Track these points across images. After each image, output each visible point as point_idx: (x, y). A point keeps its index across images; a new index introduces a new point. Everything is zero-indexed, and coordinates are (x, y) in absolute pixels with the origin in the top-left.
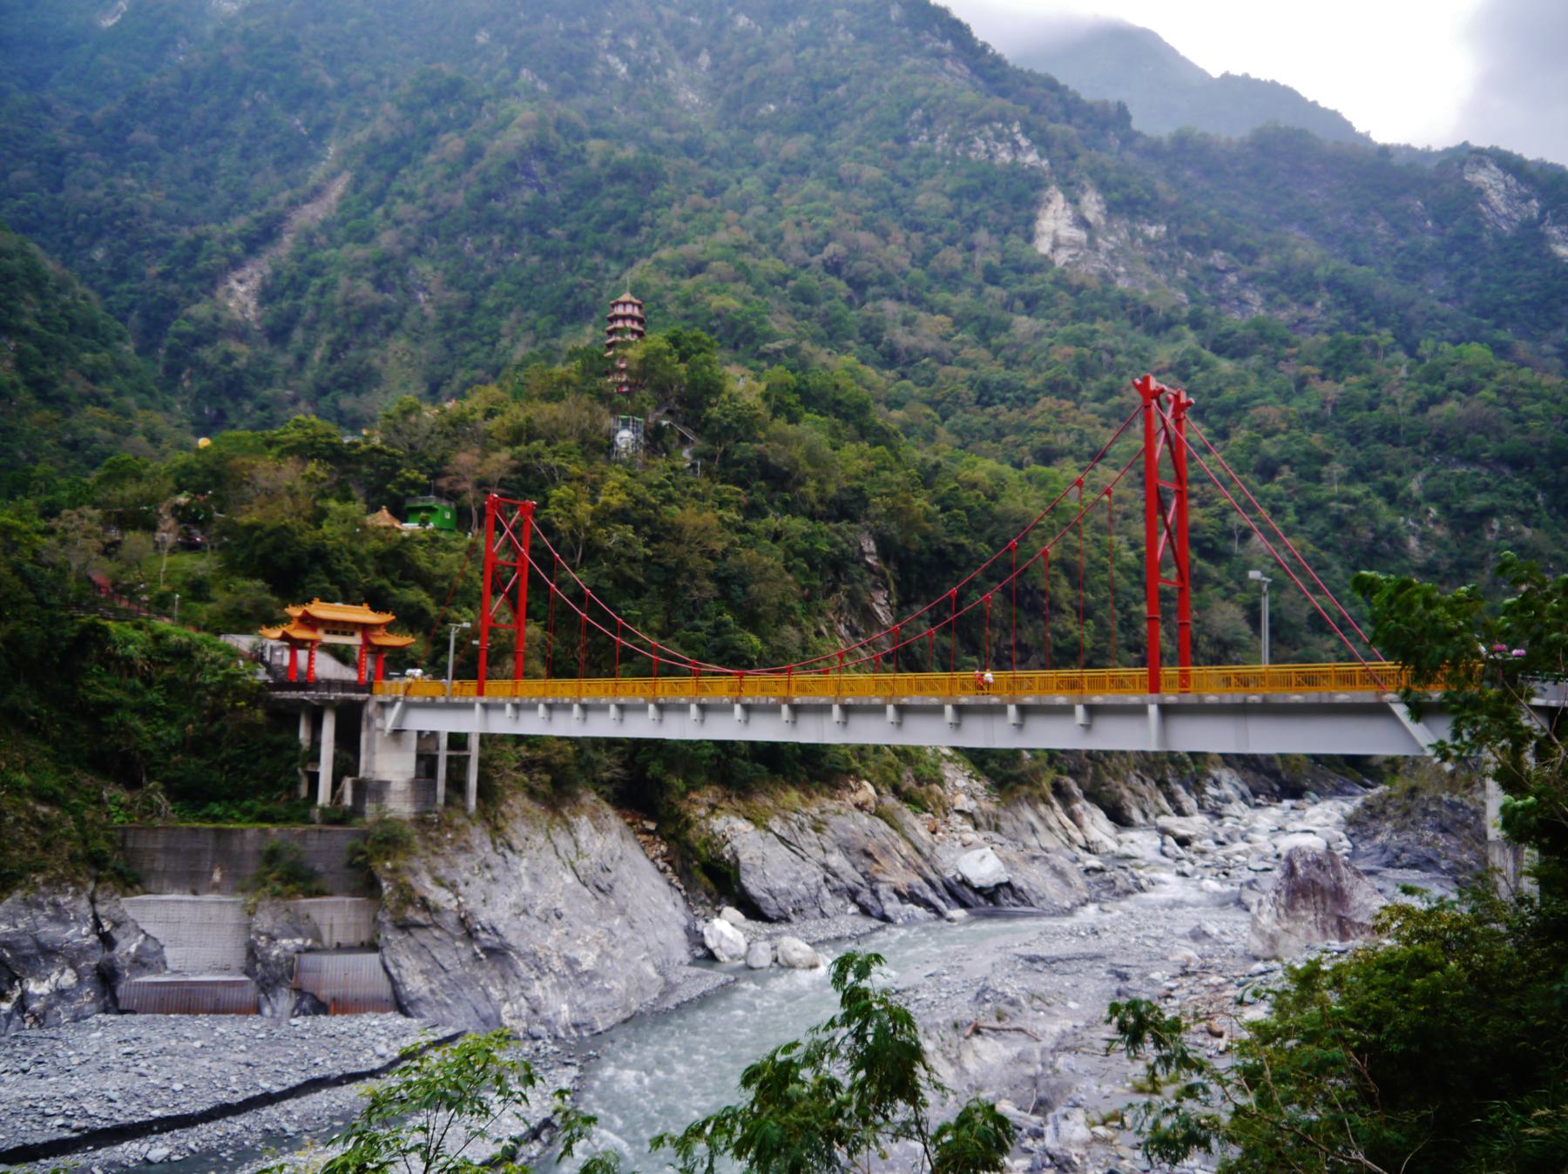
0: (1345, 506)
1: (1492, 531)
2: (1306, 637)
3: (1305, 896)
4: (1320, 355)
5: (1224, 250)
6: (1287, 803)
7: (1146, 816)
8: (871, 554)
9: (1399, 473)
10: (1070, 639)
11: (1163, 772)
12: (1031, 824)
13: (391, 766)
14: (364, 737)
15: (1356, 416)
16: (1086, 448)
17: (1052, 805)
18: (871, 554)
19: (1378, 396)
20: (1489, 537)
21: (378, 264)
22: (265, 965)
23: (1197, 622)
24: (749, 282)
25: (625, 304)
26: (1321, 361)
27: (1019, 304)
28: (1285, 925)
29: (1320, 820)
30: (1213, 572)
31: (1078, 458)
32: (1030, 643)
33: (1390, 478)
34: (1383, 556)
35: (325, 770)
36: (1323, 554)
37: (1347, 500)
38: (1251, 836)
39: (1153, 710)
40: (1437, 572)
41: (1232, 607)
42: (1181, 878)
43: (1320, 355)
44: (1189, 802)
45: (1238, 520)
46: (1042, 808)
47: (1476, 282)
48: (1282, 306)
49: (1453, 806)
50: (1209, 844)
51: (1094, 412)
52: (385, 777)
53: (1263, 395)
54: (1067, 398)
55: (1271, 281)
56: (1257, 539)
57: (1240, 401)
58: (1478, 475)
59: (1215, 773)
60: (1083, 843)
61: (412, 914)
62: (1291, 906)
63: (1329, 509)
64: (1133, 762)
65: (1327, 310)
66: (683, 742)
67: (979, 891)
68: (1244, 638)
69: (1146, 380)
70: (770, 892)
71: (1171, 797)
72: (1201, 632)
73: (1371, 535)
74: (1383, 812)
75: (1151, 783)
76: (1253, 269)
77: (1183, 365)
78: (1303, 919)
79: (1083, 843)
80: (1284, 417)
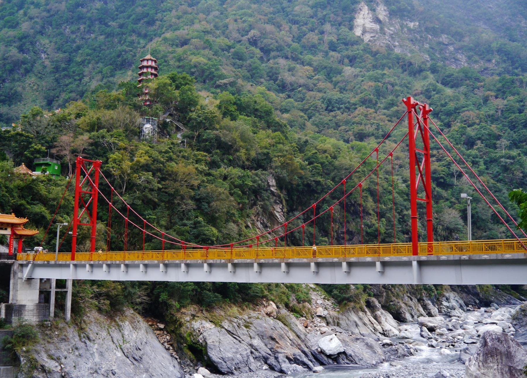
0: (508, 160)
2: (490, 226)
4: (495, 86)
5: (447, 34)
6: (483, 309)
7: (413, 317)
8: (273, 186)
10: (373, 228)
11: (421, 295)
12: (356, 322)
15: (513, 116)
16: (381, 132)
17: (366, 312)
18: (273, 186)
19: (523, 106)
21: (20, 39)
23: (437, 219)
24: (211, 49)
25: (148, 60)
26: (495, 89)
27: (346, 61)
28: (482, 371)
30: (444, 193)
31: (377, 138)
32: (354, 230)
36: (498, 184)
37: (509, 157)
38: (465, 326)
39: (415, 263)
41: (454, 211)
42: (431, 348)
43: (495, 86)
44: (434, 310)
45: (455, 167)
46: (361, 314)
48: (476, 62)
50: (444, 330)
51: (384, 115)
52: (23, 303)
53: (467, 106)
54: (371, 108)
55: (471, 49)
57: (456, 109)
59: (447, 295)
60: (381, 331)
62: (485, 361)
63: (500, 162)
64: (406, 290)
65: (498, 64)
67: (329, 356)
68: (459, 226)
70: (223, 359)
71: (425, 307)
72: (439, 224)
73: (521, 175)
75: (415, 300)
76: (462, 43)
77: (427, 90)
78: (491, 368)
79: (381, 331)
80: (478, 117)
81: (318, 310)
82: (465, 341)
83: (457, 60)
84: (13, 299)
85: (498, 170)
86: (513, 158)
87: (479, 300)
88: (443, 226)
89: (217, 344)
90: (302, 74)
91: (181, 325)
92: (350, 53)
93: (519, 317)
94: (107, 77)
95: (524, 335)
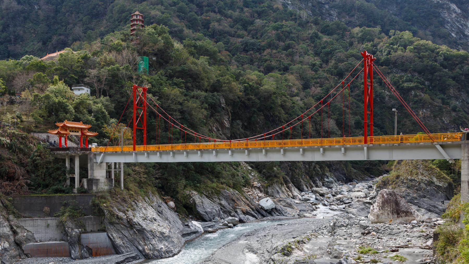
3: (387, 203)
13: (99, 174)
14: (89, 165)
22: (71, 237)
24: (162, 5)
25: (137, 15)
27: (256, 15)
29: (361, 187)
31: (280, 70)
35: (77, 176)
39: (365, 148)
41: (331, 120)
44: (320, 183)
47: (406, 8)
48: (344, 17)
50: (330, 195)
52: (98, 178)
60: (292, 196)
61: (114, 220)
66: (209, 163)
67: (266, 211)
69: (365, 52)
70: (206, 212)
77: (311, 38)
81: (254, 183)
83: (331, 15)
84: (91, 176)
89: (201, 204)
90: (225, 25)
91: (178, 193)
92: (259, 10)
94: (86, 24)
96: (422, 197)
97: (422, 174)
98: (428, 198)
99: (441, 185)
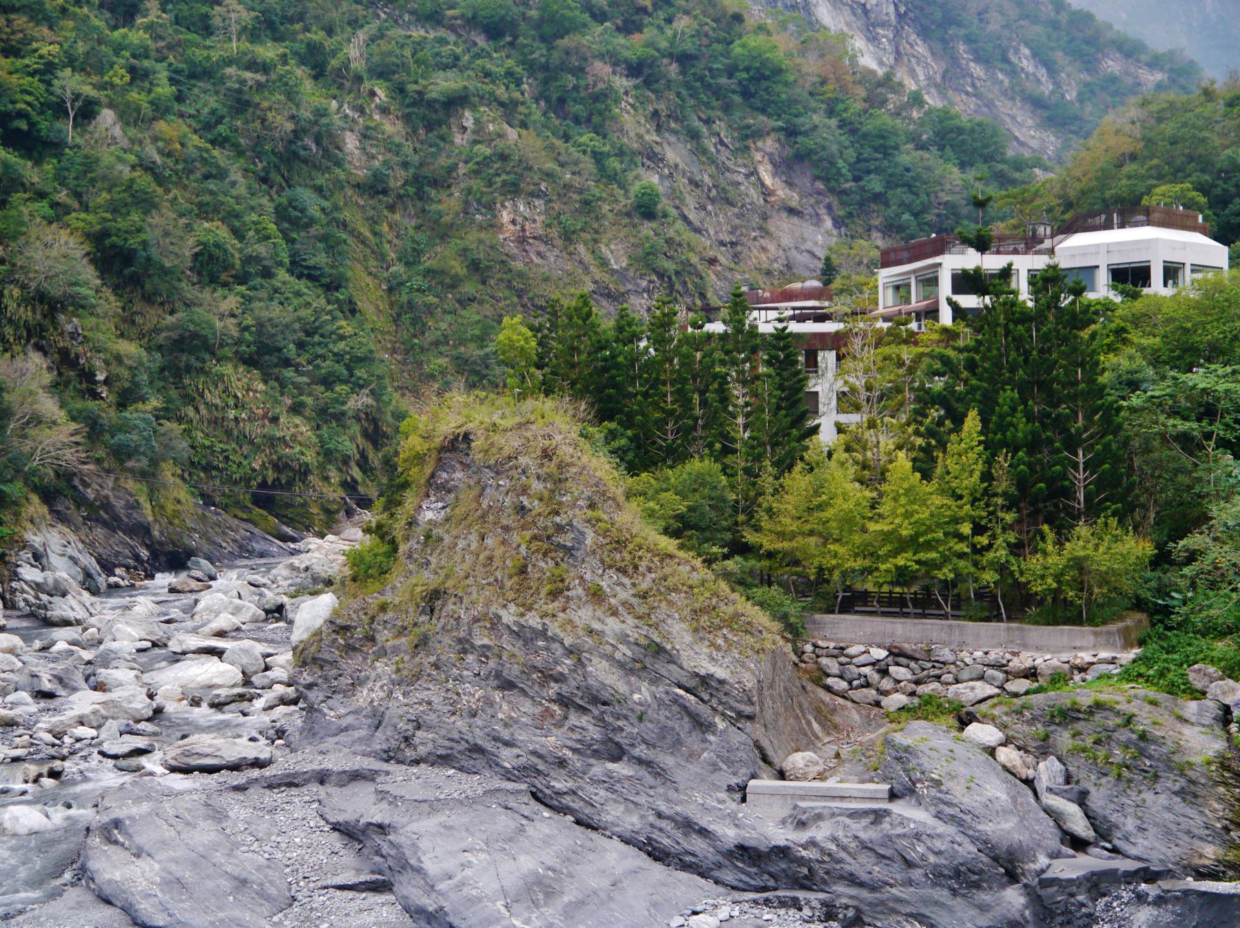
0: (248, 75)
1: (465, 129)
6: (164, 579)
9: (330, 31)
20: (458, 139)
33: (317, 36)
34: (305, 162)
36: (216, 153)
37: (252, 65)
40: (385, 192)
41: (64, 235)
45: (70, 83)
49: (522, 635)
56: (107, 116)
58: (442, 41)
59: (36, 540)
63: (222, 81)
73: (289, 126)
74: (372, 639)
82: (106, 747)
85: (214, 105)
86: (265, 68)
87: (148, 547)
88: (23, 287)
93: (327, 656)
95: (346, 729)
96: (596, 754)
97: (597, 596)
98: (640, 761)
99: (720, 673)
